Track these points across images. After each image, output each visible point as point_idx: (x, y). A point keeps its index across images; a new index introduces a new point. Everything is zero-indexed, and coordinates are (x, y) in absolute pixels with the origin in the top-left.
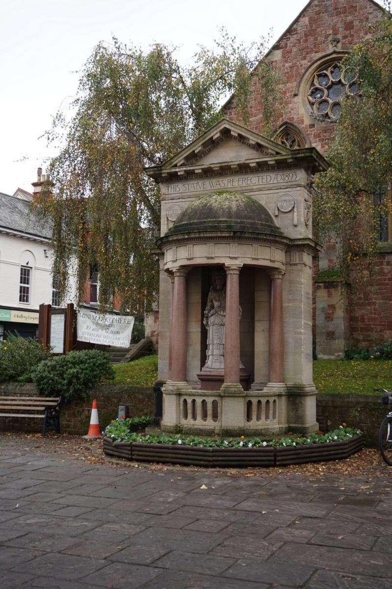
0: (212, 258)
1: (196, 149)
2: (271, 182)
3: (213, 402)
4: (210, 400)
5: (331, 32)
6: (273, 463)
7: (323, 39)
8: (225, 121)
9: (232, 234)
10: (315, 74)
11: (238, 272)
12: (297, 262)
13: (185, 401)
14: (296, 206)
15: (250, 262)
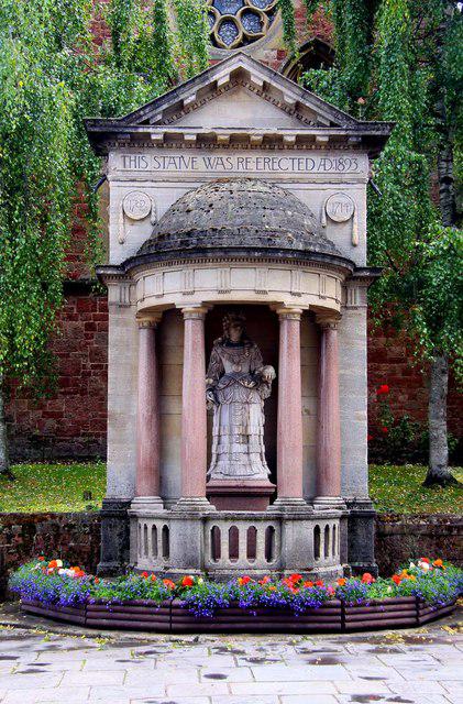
1: (187, 98)
6: (339, 625)
8: (241, 57)
12: (358, 304)
15: (214, 297)
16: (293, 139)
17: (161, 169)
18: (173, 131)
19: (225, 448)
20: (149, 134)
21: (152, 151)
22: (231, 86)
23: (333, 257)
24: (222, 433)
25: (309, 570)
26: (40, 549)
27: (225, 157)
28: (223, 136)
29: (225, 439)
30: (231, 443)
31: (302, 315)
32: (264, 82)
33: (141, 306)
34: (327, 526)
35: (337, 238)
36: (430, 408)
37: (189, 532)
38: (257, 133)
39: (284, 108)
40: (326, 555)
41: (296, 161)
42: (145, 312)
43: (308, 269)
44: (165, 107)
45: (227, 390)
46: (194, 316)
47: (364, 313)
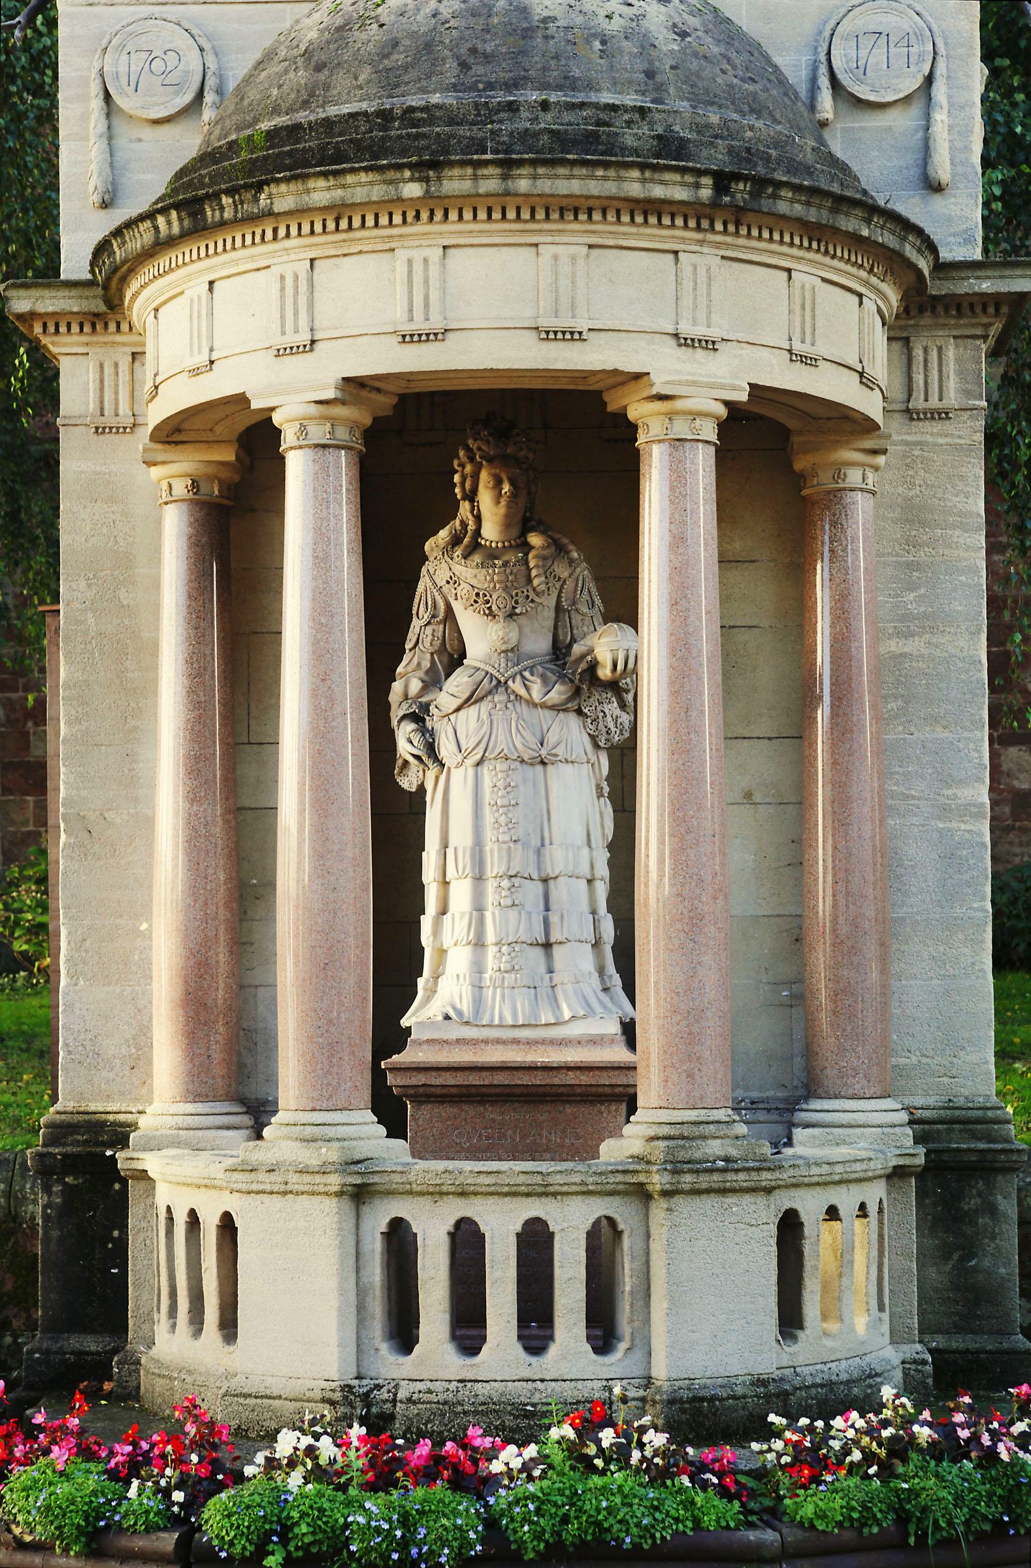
0: (573, 336)
3: (452, 1235)
4: (570, 1225)
9: (706, 193)
11: (710, 432)
12: (953, 399)
13: (399, 1238)
23: (841, 203)
31: (724, 427)
33: (157, 413)
35: (872, 155)
42: (175, 433)
43: (743, 245)
46: (318, 433)
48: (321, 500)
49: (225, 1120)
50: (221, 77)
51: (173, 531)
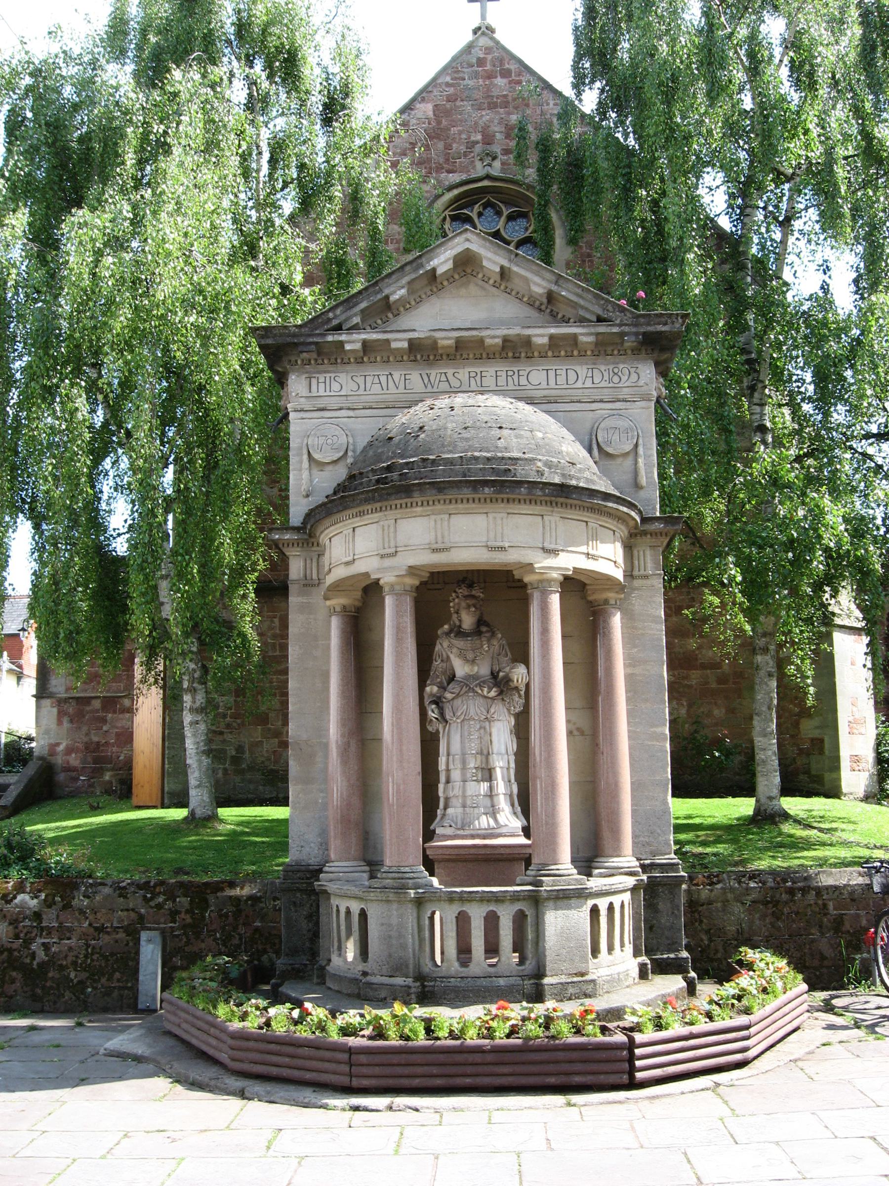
1: (395, 292)
2: (579, 384)
5: (479, 137)
7: (463, 148)
10: (447, 213)
14: (641, 441)
15: (425, 559)
16: (545, 340)
17: (361, 392)
18: (375, 336)
19: (455, 790)
20: (341, 344)
21: (348, 367)
22: (456, 277)
24: (451, 767)
25: (582, 975)
26: (215, 931)
27: (450, 372)
28: (446, 341)
29: (456, 775)
30: (464, 781)
32: (502, 267)
33: (330, 580)
34: (611, 904)
36: (755, 723)
37: (394, 921)
38: (493, 337)
39: (531, 303)
40: (611, 949)
41: (552, 374)
44: (363, 305)
45: (458, 702)
47: (658, 584)
48: (398, 614)
49: (359, 869)
50: (354, 445)
51: (335, 626)
